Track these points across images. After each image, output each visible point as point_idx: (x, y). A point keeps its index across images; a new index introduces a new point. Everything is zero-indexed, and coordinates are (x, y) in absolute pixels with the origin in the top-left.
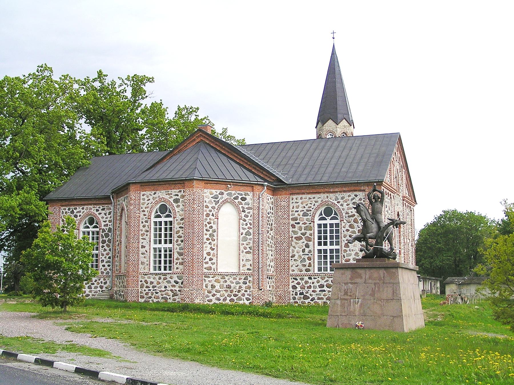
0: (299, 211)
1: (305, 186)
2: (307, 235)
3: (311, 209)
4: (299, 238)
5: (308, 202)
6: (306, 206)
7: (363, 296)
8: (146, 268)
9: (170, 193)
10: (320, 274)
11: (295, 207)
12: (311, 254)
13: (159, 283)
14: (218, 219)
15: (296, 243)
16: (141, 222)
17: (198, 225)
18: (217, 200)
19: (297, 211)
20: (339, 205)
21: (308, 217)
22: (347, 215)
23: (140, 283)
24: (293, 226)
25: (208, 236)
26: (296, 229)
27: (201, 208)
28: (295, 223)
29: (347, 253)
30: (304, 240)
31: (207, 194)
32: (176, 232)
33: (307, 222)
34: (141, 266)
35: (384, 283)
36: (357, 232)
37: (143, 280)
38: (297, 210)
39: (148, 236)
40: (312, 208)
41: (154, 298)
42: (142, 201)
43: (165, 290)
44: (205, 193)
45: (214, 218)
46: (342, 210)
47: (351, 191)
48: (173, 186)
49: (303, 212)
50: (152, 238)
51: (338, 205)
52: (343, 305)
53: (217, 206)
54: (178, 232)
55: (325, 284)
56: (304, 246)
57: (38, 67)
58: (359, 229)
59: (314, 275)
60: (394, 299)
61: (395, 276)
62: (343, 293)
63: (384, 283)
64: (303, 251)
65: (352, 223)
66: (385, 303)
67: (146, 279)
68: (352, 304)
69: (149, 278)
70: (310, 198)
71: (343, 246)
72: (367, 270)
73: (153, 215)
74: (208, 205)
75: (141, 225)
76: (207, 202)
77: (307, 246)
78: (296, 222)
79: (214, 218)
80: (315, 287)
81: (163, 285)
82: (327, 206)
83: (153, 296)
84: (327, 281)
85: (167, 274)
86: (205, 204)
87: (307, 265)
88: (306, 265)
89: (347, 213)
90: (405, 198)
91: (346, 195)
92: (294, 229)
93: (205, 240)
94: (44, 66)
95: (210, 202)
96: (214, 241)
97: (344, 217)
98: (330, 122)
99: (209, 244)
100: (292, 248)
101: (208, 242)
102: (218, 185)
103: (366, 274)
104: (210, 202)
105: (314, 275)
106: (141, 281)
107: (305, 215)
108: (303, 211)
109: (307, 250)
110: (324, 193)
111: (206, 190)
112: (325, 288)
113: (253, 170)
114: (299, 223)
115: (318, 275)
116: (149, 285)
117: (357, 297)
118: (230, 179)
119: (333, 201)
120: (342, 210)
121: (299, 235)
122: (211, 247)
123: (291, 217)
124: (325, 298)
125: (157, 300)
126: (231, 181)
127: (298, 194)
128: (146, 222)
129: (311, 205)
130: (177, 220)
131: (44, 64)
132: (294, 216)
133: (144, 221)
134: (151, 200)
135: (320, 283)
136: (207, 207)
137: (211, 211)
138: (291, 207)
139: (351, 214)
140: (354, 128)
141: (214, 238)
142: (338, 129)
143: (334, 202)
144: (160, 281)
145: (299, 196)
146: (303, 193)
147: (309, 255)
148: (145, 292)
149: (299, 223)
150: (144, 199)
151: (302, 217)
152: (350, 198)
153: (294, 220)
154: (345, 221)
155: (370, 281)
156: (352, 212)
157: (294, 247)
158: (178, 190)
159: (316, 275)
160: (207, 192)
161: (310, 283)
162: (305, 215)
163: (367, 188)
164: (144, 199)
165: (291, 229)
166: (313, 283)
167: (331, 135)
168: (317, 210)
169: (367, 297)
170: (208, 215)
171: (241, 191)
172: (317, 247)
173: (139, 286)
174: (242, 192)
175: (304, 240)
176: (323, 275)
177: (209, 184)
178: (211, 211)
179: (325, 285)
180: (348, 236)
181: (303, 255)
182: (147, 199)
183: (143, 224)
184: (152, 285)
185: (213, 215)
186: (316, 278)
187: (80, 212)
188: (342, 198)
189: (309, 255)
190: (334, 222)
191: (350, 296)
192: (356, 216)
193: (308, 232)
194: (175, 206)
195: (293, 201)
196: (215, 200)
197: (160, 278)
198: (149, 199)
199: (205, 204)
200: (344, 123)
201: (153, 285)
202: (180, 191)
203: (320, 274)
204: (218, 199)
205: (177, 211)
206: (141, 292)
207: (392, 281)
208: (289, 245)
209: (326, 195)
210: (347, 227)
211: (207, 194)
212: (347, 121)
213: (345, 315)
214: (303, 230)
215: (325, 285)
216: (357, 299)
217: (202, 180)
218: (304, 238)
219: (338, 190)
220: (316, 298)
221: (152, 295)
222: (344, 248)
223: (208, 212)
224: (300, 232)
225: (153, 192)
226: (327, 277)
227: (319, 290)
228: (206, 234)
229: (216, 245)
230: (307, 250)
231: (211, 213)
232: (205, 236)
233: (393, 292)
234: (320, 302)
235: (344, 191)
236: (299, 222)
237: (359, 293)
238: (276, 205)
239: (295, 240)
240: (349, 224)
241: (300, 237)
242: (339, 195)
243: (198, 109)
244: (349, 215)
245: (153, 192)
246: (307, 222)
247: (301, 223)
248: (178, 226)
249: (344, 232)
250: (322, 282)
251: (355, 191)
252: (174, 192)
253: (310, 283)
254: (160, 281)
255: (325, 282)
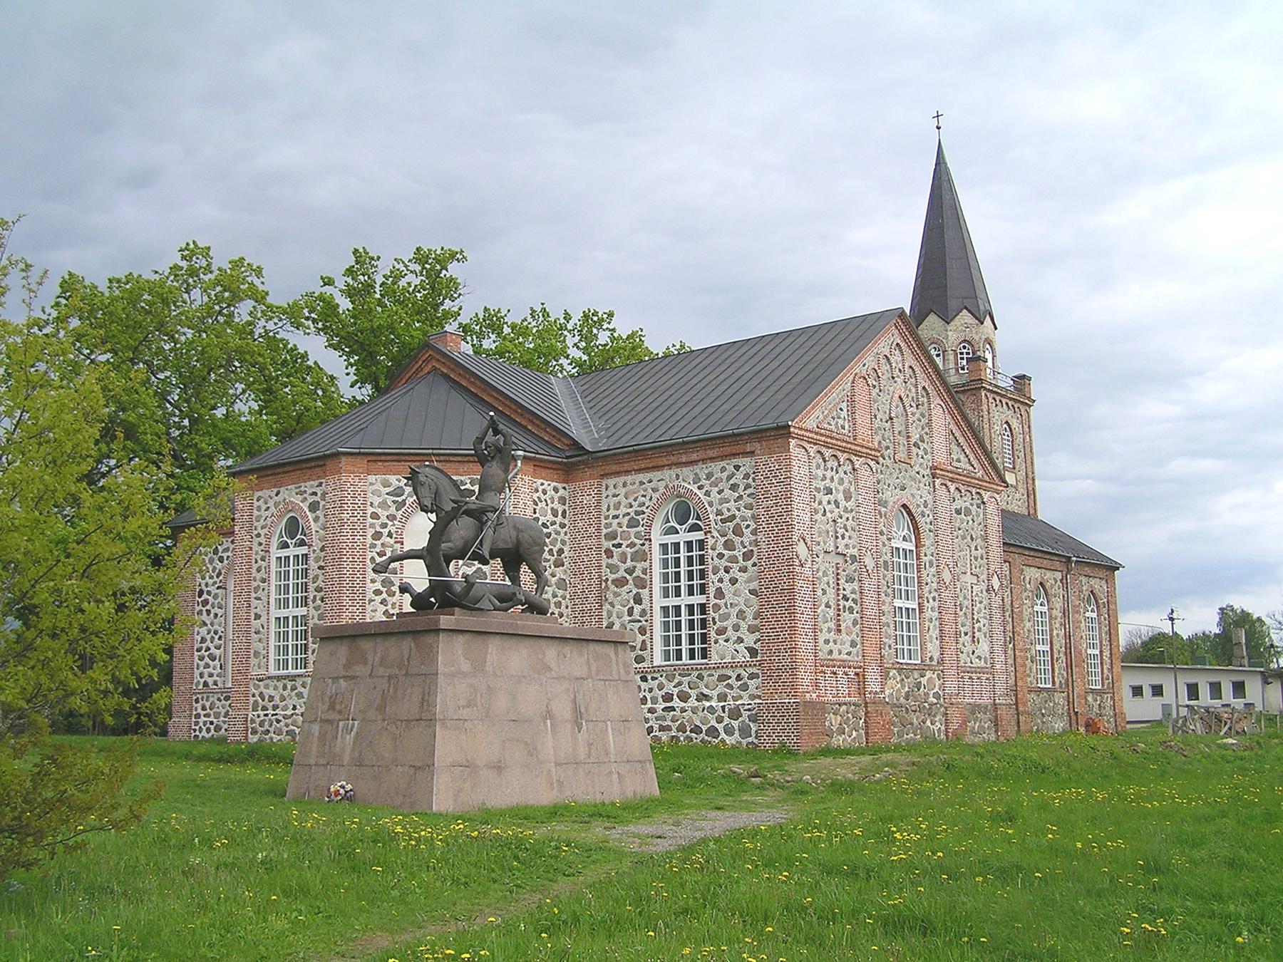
0: (621, 516)
1: (626, 453)
2: (638, 573)
3: (644, 508)
4: (621, 582)
5: (639, 491)
6: (633, 503)
7: (363, 712)
8: (262, 664)
9: (302, 489)
10: (664, 669)
11: (612, 507)
12: (646, 618)
13: (283, 699)
14: (402, 544)
15: (616, 595)
16: (253, 561)
17: (351, 559)
18: (400, 499)
19: (616, 517)
20: (700, 494)
21: (640, 528)
22: (719, 517)
23: (252, 700)
24: (609, 554)
25: (378, 586)
26: (615, 561)
27: (359, 520)
28: (613, 546)
29: (721, 612)
30: (631, 585)
31: (375, 487)
32: (313, 579)
33: (637, 541)
34: (253, 661)
35: (406, 675)
36: (740, 559)
37: (257, 693)
38: (617, 513)
39: (266, 591)
40: (647, 505)
41: (274, 733)
42: (256, 513)
43: (292, 715)
44: (371, 484)
45: (392, 541)
46: (707, 506)
47: (726, 456)
48: (309, 472)
49: (627, 518)
50: (273, 596)
51: (700, 495)
52: (323, 737)
53: (400, 512)
54: (316, 578)
55: (676, 691)
56: (632, 601)
57: (179, 251)
58: (745, 550)
59: (652, 670)
60: (421, 719)
61: (429, 656)
62: (326, 707)
63: (406, 675)
64: (630, 612)
65: (731, 536)
66: (404, 730)
67: (262, 689)
68: (340, 734)
69: (267, 687)
70: (642, 483)
71: (712, 596)
72: (379, 640)
73: (275, 543)
74: (379, 511)
75: (255, 566)
76: (376, 504)
77: (638, 600)
78: (614, 542)
79: (392, 543)
80: (654, 701)
81: (290, 703)
82: (678, 499)
83: (272, 729)
84: (680, 684)
85: (295, 676)
86: (370, 510)
87: (638, 647)
88: (635, 647)
89: (719, 513)
90: (938, 471)
91: (715, 467)
92: (610, 561)
93: (370, 595)
94: (192, 246)
95: (383, 505)
96: (394, 595)
97: (713, 523)
98: (932, 318)
99: (381, 603)
100: (607, 606)
101: (379, 598)
102: (403, 463)
103: (375, 651)
104: (383, 505)
105: (652, 670)
106: (254, 696)
107: (633, 523)
108: (628, 514)
109: (637, 609)
110: (670, 466)
111: (371, 478)
112: (676, 703)
113: (529, 427)
114: (619, 545)
115: (661, 669)
116: (266, 703)
117: (351, 716)
118: (429, 449)
119: (688, 486)
120: (707, 506)
121: (621, 573)
122: (387, 610)
123: (604, 531)
124: (674, 726)
125: (279, 738)
126: (431, 451)
127: (618, 474)
128: (263, 559)
129: (644, 498)
130: (314, 551)
131: (191, 243)
132: (610, 530)
133: (259, 558)
134: (273, 509)
135: (665, 690)
136: (375, 516)
137: (384, 526)
138: (604, 508)
139: (727, 514)
140: (996, 328)
141: (392, 588)
142: (950, 333)
143: (691, 488)
144: (285, 693)
145: (620, 480)
146: (628, 472)
147: (640, 621)
148: (258, 720)
149: (619, 545)
150: (259, 509)
151: (626, 529)
152: (725, 474)
153: (610, 540)
154: (715, 534)
155: (381, 671)
156: (729, 510)
157: (612, 604)
158: (317, 483)
159: (654, 671)
160: (374, 482)
161: (645, 691)
162: (633, 523)
163: (757, 445)
164: (259, 509)
165: (605, 561)
166: (651, 690)
167: (935, 348)
168: (655, 510)
169: (372, 713)
170: (377, 536)
171: (462, 475)
172: (659, 602)
173: (251, 707)
174: (463, 478)
175: (631, 585)
176: (670, 670)
177: (380, 464)
178: (384, 526)
179: (675, 694)
180: (723, 571)
181: (630, 621)
182: (264, 507)
183: (257, 565)
184: (271, 704)
185: (390, 535)
186: (656, 679)
187: (226, 550)
188: (709, 476)
189: (640, 621)
190: (696, 536)
191: (340, 712)
192: (738, 519)
193: (640, 566)
194: (311, 520)
195: (609, 493)
196: (397, 499)
197: (285, 688)
198: (268, 508)
199: (370, 510)
200: (965, 317)
201: (273, 703)
202: (320, 485)
203: (664, 669)
204: (403, 497)
205: (313, 530)
206: (252, 719)
207: (424, 669)
208: (601, 600)
209: (673, 472)
210: (720, 549)
211: (375, 487)
212: (972, 314)
213: (324, 765)
214: (629, 560)
215: (675, 694)
216: (351, 722)
217: (359, 454)
218: (631, 582)
219: (698, 458)
220: (656, 727)
221: (271, 726)
222: (713, 601)
223: (378, 529)
224: (623, 567)
225: (275, 490)
226: (679, 675)
227: (663, 707)
228: (373, 581)
229: (397, 606)
230: (637, 609)
231: (385, 531)
232: (371, 585)
233: (423, 699)
234: (664, 737)
235: (712, 459)
236: (621, 542)
237: (357, 703)
238: (570, 506)
239: (612, 587)
240: (723, 540)
241: (625, 580)
242: (701, 469)
243: (611, 315)
244: (723, 517)
245: (275, 490)
246: (637, 541)
247: (625, 543)
248: (316, 566)
249: (712, 560)
250: (670, 687)
251: (735, 455)
252: (310, 486)
253: (645, 691)
254: (285, 693)
255: (674, 687)
